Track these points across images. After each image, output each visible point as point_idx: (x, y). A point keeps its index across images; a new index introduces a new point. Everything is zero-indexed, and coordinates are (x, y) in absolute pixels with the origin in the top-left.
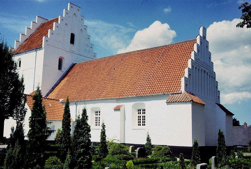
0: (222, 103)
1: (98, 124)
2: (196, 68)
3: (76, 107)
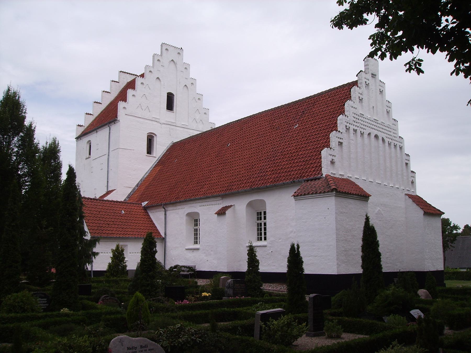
0: (420, 192)
1: (263, 236)
2: (395, 146)
3: (165, 214)
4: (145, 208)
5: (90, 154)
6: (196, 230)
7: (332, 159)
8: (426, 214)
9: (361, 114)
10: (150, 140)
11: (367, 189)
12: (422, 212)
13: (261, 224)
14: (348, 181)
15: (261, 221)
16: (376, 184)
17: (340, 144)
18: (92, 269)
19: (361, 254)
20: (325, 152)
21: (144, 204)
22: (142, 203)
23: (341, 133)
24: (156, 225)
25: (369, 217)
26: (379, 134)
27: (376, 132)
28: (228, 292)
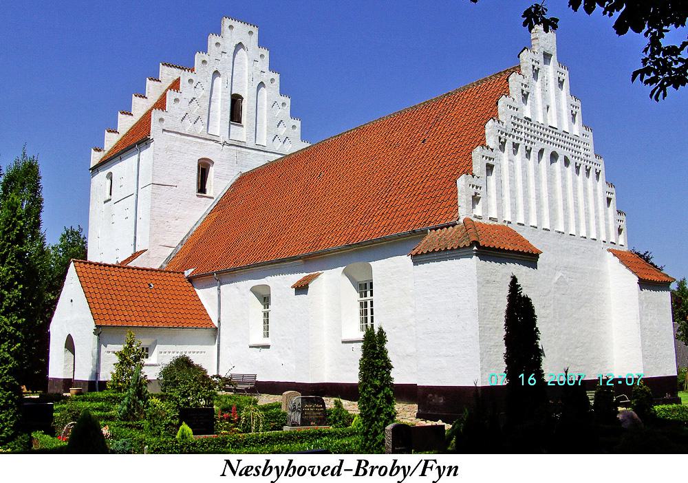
4: (190, 279)
5: (111, 194)
6: (266, 315)
7: (476, 193)
8: (644, 284)
9: (525, 118)
10: (203, 169)
11: (535, 241)
12: (635, 279)
13: (366, 303)
14: (506, 231)
15: (366, 298)
16: (554, 232)
17: (490, 168)
18: (97, 378)
19: (504, 349)
20: (462, 182)
21: (187, 273)
22: (185, 272)
23: (492, 150)
24: (206, 306)
25: (520, 286)
26: (559, 150)
27: (553, 148)
28: (292, 418)
